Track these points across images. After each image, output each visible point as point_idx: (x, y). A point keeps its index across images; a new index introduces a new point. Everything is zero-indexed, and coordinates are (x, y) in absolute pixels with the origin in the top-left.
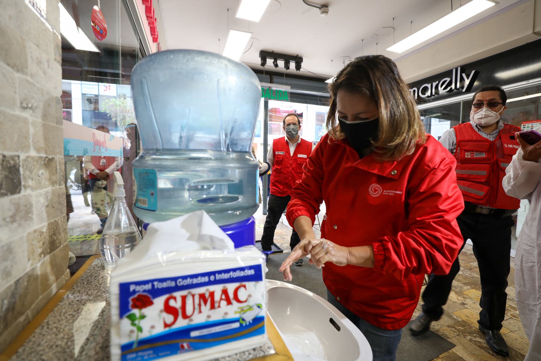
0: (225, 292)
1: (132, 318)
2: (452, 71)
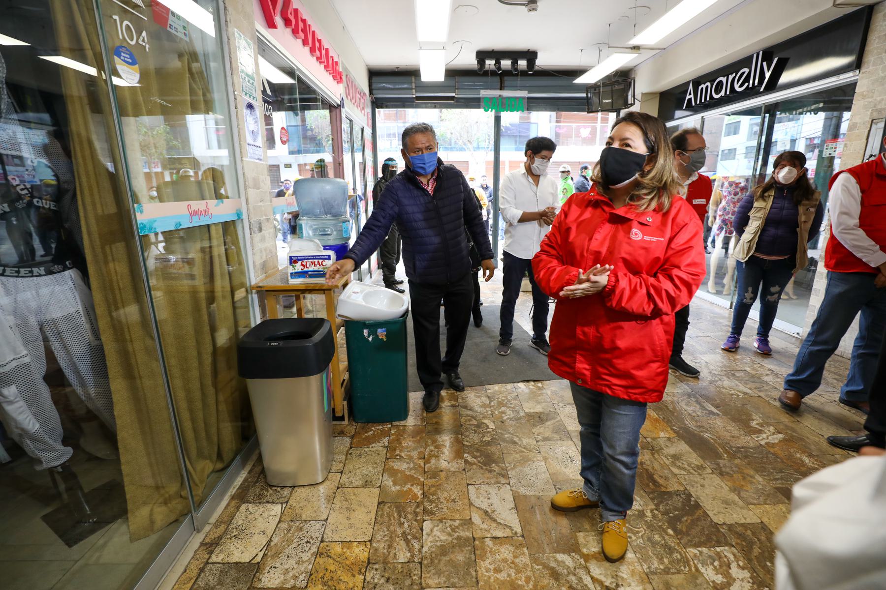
0: (318, 262)
1: (293, 266)
2: (752, 56)
